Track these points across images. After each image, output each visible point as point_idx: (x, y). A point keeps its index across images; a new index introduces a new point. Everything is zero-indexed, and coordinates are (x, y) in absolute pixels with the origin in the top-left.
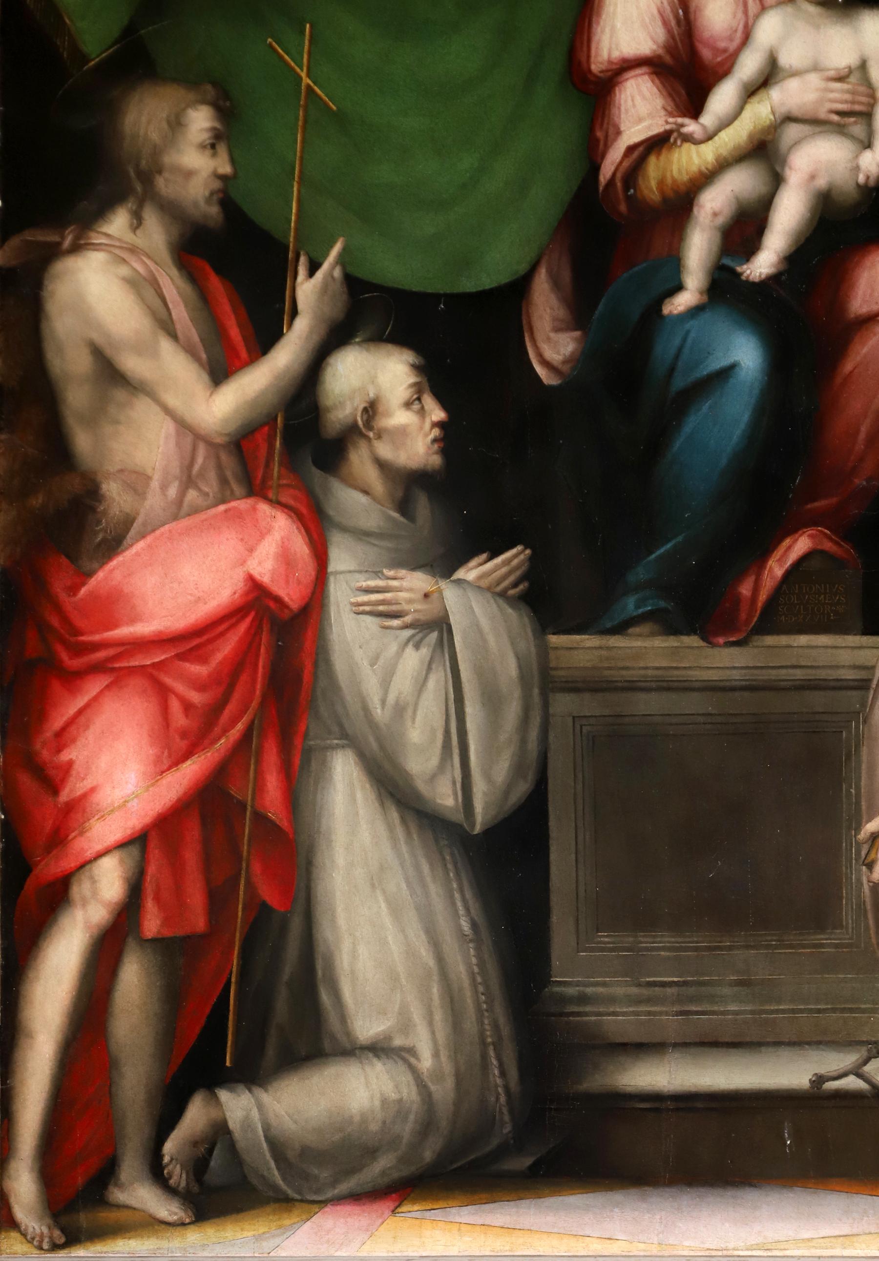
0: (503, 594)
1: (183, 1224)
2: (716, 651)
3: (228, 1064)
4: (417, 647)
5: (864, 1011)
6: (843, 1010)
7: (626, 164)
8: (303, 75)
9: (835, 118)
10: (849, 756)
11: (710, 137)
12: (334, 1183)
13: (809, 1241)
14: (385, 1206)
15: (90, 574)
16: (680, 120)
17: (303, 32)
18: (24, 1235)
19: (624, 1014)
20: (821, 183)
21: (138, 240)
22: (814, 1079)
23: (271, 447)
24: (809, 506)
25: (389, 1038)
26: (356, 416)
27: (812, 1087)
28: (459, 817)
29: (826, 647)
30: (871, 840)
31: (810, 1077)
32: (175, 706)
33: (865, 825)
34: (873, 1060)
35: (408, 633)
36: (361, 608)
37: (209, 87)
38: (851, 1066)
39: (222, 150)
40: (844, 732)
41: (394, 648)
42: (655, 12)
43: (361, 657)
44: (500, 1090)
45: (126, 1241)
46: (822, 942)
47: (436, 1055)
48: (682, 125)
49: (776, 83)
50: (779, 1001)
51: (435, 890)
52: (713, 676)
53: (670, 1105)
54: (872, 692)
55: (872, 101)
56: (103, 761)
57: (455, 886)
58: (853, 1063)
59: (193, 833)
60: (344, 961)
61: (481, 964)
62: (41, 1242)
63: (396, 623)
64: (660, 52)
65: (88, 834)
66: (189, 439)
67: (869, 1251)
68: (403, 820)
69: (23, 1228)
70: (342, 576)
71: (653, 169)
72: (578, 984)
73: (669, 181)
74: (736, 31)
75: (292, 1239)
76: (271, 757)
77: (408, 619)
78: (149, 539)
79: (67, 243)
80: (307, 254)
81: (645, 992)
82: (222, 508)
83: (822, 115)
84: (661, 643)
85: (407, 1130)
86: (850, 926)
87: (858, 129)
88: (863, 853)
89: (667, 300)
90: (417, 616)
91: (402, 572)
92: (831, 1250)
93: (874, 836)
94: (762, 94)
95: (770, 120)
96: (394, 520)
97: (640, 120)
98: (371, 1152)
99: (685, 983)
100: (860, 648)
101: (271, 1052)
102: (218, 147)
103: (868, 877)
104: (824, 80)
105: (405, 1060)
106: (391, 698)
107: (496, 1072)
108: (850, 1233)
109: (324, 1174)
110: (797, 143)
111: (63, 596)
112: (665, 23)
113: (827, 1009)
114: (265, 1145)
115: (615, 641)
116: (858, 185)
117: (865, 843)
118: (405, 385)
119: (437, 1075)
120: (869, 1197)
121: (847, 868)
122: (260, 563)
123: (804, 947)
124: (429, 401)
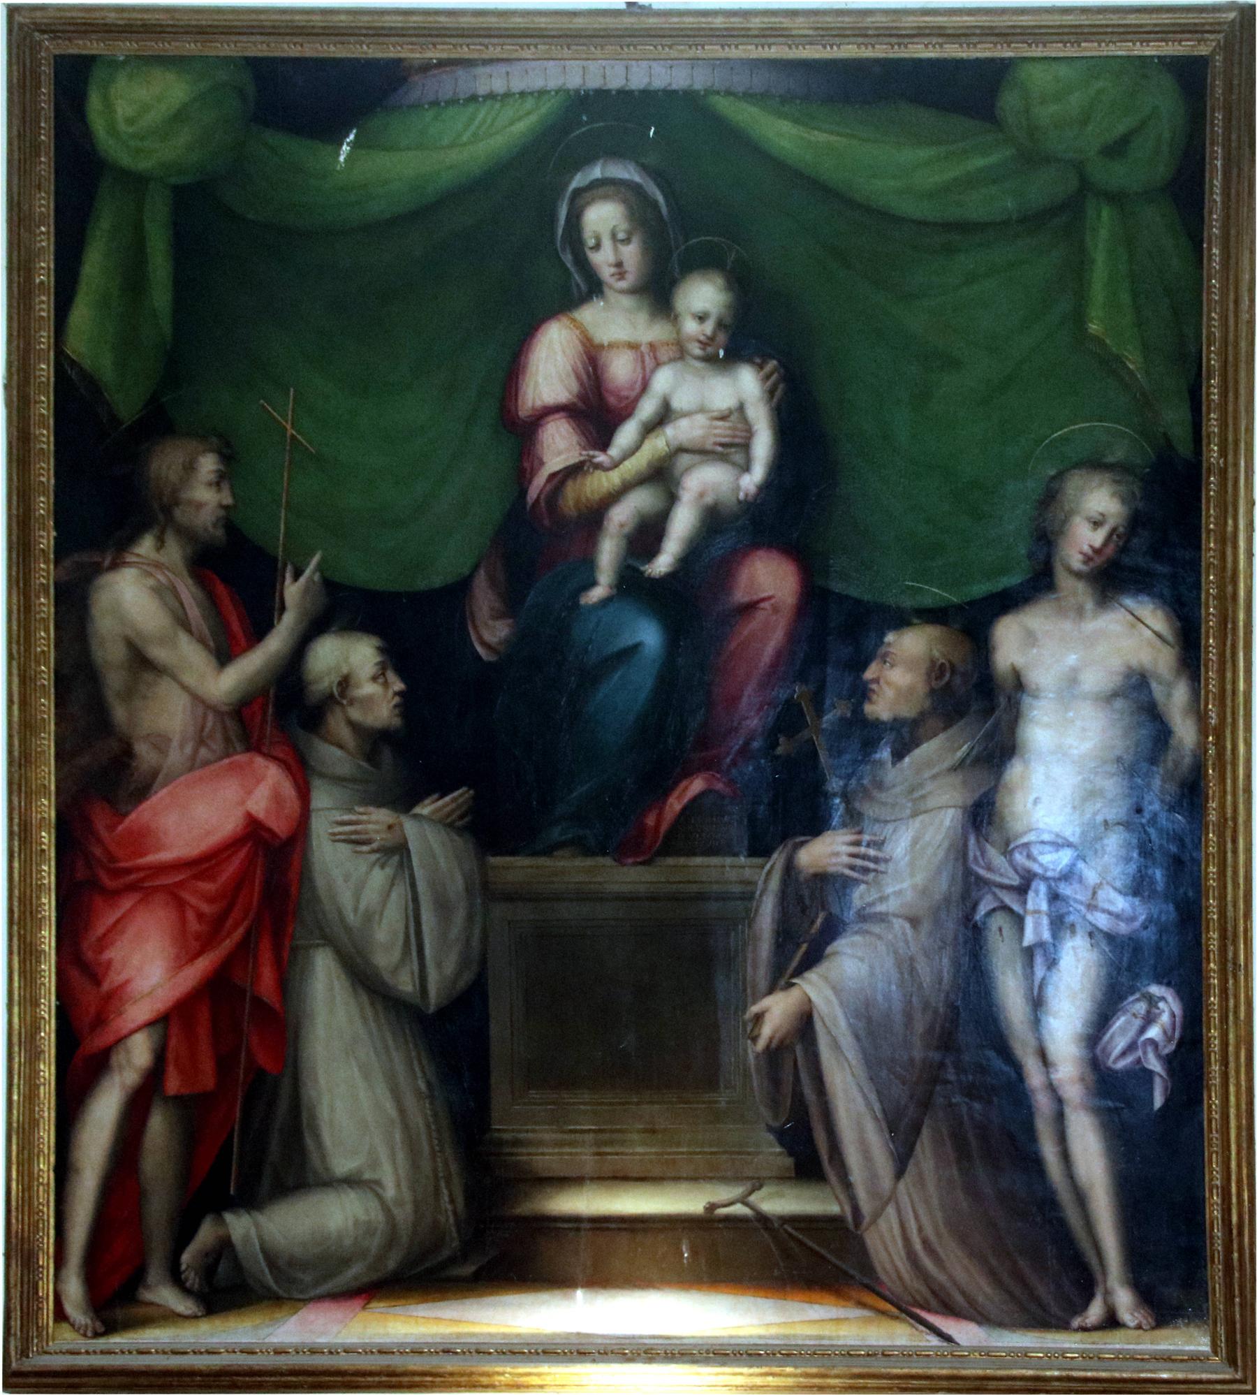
0: (451, 826)
1: (196, 1317)
2: (625, 869)
3: (232, 1192)
4: (382, 867)
5: (749, 1154)
7: (548, 488)
8: (289, 427)
9: (719, 449)
11: (616, 465)
12: (317, 1283)
14: (357, 1303)
15: (126, 815)
16: (591, 453)
17: (288, 394)
18: (73, 1325)
19: (550, 1154)
20: (709, 499)
21: (162, 558)
23: (265, 713)
25: (359, 1172)
26: (332, 688)
28: (418, 1001)
32: (191, 916)
35: (374, 857)
36: (338, 837)
37: (214, 439)
39: (225, 486)
41: (363, 868)
42: (570, 369)
43: (337, 874)
44: (450, 1213)
45: (151, 1330)
47: (398, 1185)
48: (593, 457)
50: (678, 1144)
51: (398, 1059)
52: (625, 888)
53: (588, 1226)
56: (136, 960)
57: (414, 1054)
59: (204, 1016)
60: (324, 1113)
61: (435, 1115)
62: (85, 1331)
63: (365, 848)
64: (575, 400)
65: (124, 1016)
66: (200, 710)
68: (372, 1004)
69: (72, 1320)
70: (321, 813)
71: (571, 493)
72: (513, 1131)
73: (584, 500)
74: (635, 383)
75: (283, 1329)
76: (266, 956)
77: (375, 845)
78: (170, 788)
79: (107, 563)
80: (292, 563)
81: (566, 1136)
82: (226, 761)
83: (709, 446)
84: (579, 862)
85: (375, 1243)
87: (738, 457)
89: (583, 594)
90: (382, 843)
91: (371, 809)
94: (658, 431)
96: (360, 766)
97: (560, 453)
98: (346, 1262)
99: (600, 1131)
101: (266, 1182)
102: (222, 485)
105: (371, 1188)
106: (362, 906)
107: (446, 1199)
109: (307, 1278)
110: (688, 469)
111: (104, 833)
112: (578, 377)
114: (261, 1256)
115: (542, 861)
116: (738, 500)
118: (372, 664)
119: (399, 1203)
122: (256, 803)
124: (391, 676)
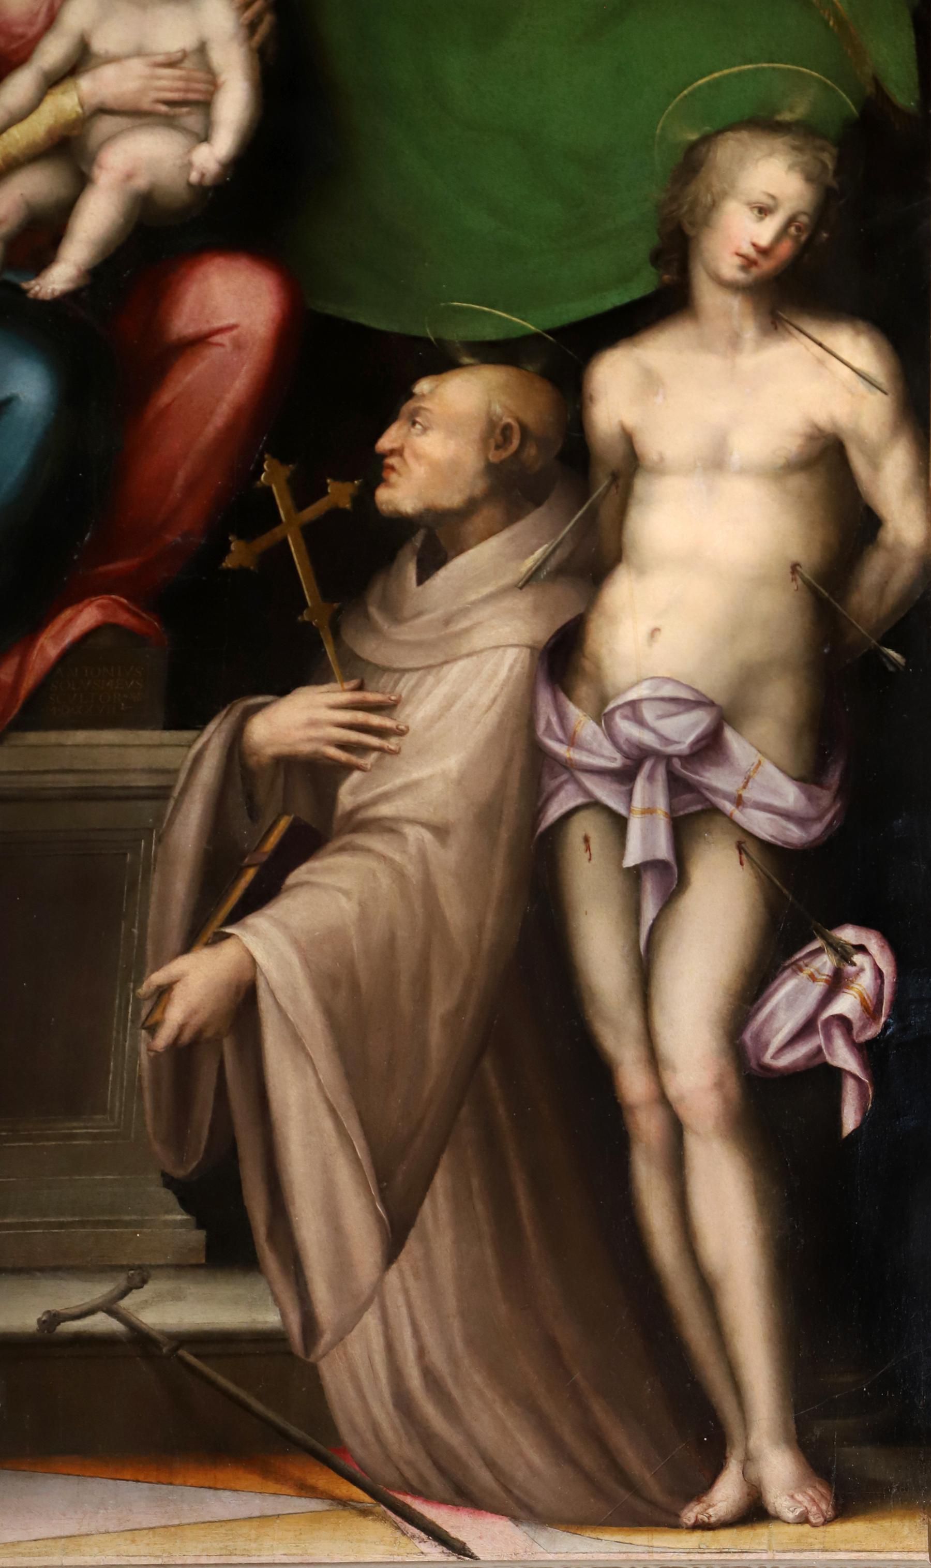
5: (127, 1224)
6: (96, 1224)
9: (163, 108)
10: (133, 885)
13: (13, 1545)
20: (141, 182)
22: (44, 1318)
24: (102, 569)
27: (40, 1330)
29: (112, 746)
30: (157, 994)
31: (40, 1316)
33: (149, 976)
34: (134, 1291)
38: (100, 1300)
40: (129, 855)
46: (74, 1131)
49: (87, 71)
54: (172, 803)
55: (211, 88)
58: (104, 1296)
67: (103, 1557)
74: (37, 14)
83: (146, 104)
86: (117, 1109)
87: (193, 120)
88: (144, 1013)
92: (46, 1558)
93: (161, 989)
94: (68, 84)
95: (77, 112)
100: (161, 746)
103: (148, 1045)
104: (149, 66)
108: (77, 1533)
110: (112, 138)
113: (72, 1223)
116: (190, 185)
117: (146, 999)
120: (110, 1481)
121: (118, 1033)
123: (48, 1138)
